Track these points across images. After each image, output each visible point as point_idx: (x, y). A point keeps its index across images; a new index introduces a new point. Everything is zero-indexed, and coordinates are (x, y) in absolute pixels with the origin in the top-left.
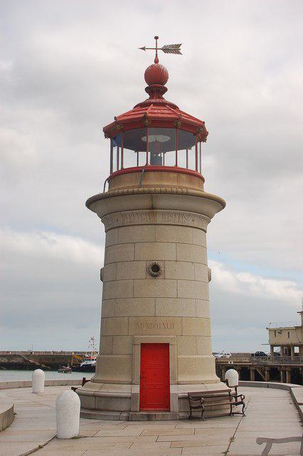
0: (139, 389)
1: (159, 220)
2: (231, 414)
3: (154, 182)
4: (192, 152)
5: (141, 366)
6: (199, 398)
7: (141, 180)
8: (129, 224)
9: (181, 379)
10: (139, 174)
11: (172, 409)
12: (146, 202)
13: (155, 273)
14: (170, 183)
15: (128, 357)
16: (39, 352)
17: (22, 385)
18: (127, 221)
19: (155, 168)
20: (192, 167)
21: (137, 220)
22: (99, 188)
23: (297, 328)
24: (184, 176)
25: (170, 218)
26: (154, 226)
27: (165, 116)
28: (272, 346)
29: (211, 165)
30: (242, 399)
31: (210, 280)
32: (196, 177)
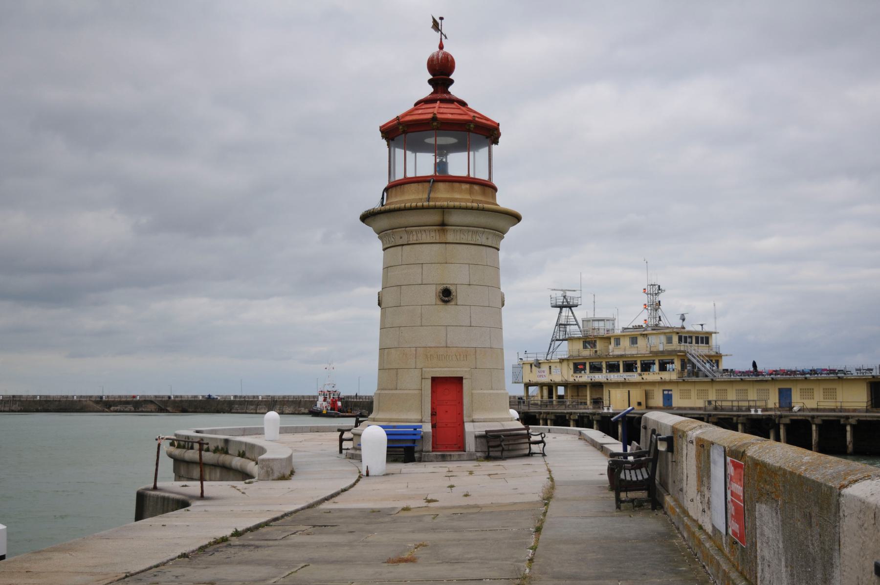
1: (450, 237)
2: (530, 454)
3: (444, 195)
6: (498, 437)
10: (426, 185)
11: (467, 449)
12: (435, 218)
14: (461, 196)
16: (181, 397)
18: (413, 239)
19: (441, 177)
20: (483, 175)
21: (425, 238)
22: (373, 202)
23: (562, 361)
24: (476, 187)
25: (462, 236)
28: (527, 386)
29: (512, 172)
31: (503, 305)
32: (488, 187)
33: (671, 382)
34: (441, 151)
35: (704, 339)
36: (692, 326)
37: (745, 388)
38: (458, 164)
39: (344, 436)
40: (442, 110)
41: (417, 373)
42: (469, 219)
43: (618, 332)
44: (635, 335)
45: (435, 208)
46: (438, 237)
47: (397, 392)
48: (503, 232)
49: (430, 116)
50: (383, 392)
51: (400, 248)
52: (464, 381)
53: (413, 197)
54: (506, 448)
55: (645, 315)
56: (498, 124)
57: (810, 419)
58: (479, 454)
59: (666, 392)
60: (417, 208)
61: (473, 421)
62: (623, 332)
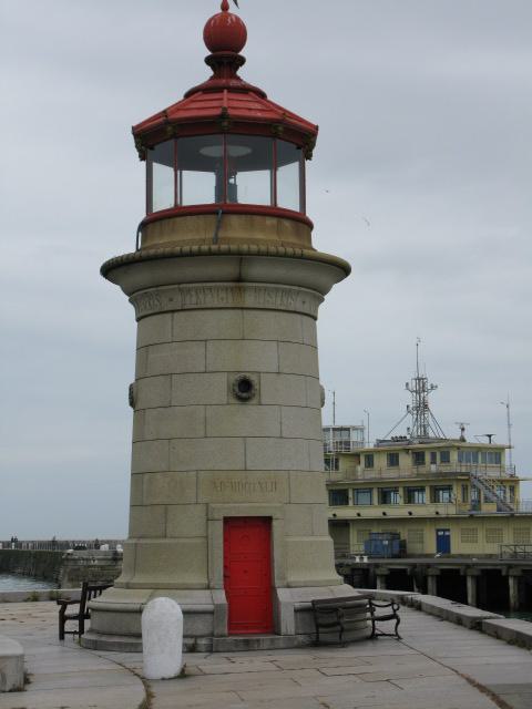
0: (224, 595)
1: (250, 299)
2: (373, 637)
4: (288, 173)
5: (225, 558)
6: (335, 610)
7: (218, 228)
8: (193, 306)
9: (292, 578)
10: (212, 218)
11: (283, 630)
12: (229, 269)
13: (244, 395)
14: (263, 236)
15: (199, 541)
17: (444, 616)
19: (225, 207)
20: (288, 201)
21: (211, 300)
22: (126, 244)
24: (287, 223)
25: (268, 298)
26: (240, 311)
27: (253, 114)
29: (336, 204)
30: (395, 611)
32: (301, 223)
33: (448, 519)
34: (224, 172)
35: (496, 454)
36: (474, 437)
37: (474, 526)
38: (252, 187)
39: (67, 612)
40: (235, 104)
41: (199, 511)
42: (279, 271)
43: (370, 446)
44: (393, 451)
45: (229, 253)
46: (230, 300)
47: (167, 541)
48: (325, 291)
49: (218, 112)
50: (142, 541)
51: (169, 316)
52: (275, 523)
53: (189, 237)
54: (345, 626)
55: (409, 420)
56: (317, 128)
57: (462, 568)
58: (301, 638)
59: (441, 533)
60: (200, 254)
61: (288, 587)
62: (377, 445)
